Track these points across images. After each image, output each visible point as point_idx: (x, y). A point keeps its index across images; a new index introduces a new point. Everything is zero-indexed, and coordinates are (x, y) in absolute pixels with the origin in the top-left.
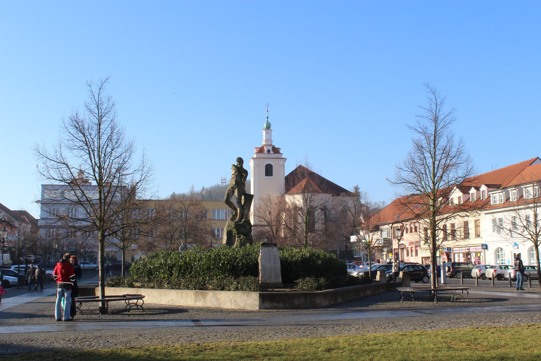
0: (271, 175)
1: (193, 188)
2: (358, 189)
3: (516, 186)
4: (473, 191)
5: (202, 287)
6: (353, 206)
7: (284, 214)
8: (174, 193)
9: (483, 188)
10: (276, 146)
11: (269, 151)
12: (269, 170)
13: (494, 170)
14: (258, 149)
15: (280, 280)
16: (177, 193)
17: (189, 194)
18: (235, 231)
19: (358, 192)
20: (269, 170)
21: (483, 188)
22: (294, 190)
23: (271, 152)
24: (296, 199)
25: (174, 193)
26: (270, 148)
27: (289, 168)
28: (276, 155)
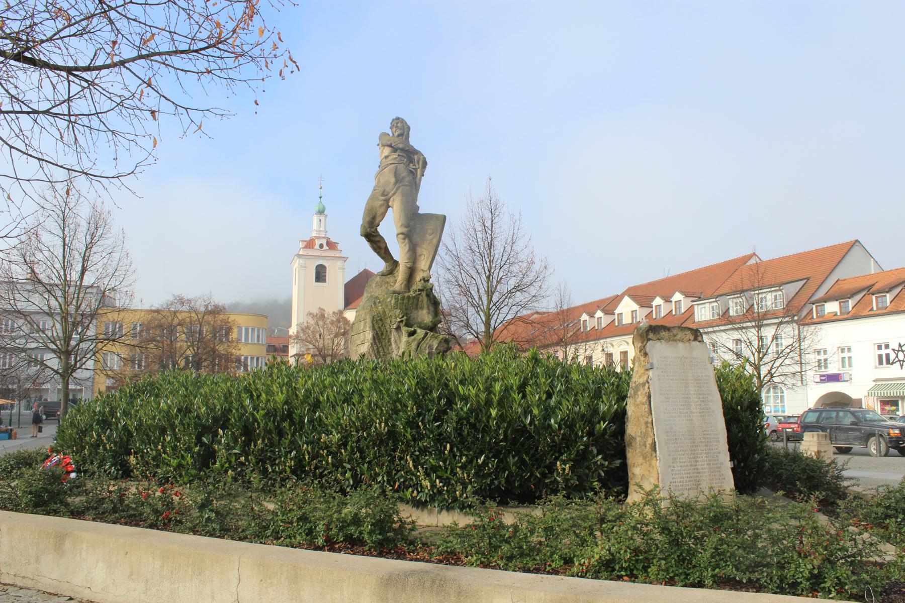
0: (324, 281)
10: (333, 240)
11: (321, 246)
12: (320, 274)
15: (729, 483)
18: (395, 316)
20: (320, 274)
23: (325, 247)
26: (324, 242)
28: (332, 253)
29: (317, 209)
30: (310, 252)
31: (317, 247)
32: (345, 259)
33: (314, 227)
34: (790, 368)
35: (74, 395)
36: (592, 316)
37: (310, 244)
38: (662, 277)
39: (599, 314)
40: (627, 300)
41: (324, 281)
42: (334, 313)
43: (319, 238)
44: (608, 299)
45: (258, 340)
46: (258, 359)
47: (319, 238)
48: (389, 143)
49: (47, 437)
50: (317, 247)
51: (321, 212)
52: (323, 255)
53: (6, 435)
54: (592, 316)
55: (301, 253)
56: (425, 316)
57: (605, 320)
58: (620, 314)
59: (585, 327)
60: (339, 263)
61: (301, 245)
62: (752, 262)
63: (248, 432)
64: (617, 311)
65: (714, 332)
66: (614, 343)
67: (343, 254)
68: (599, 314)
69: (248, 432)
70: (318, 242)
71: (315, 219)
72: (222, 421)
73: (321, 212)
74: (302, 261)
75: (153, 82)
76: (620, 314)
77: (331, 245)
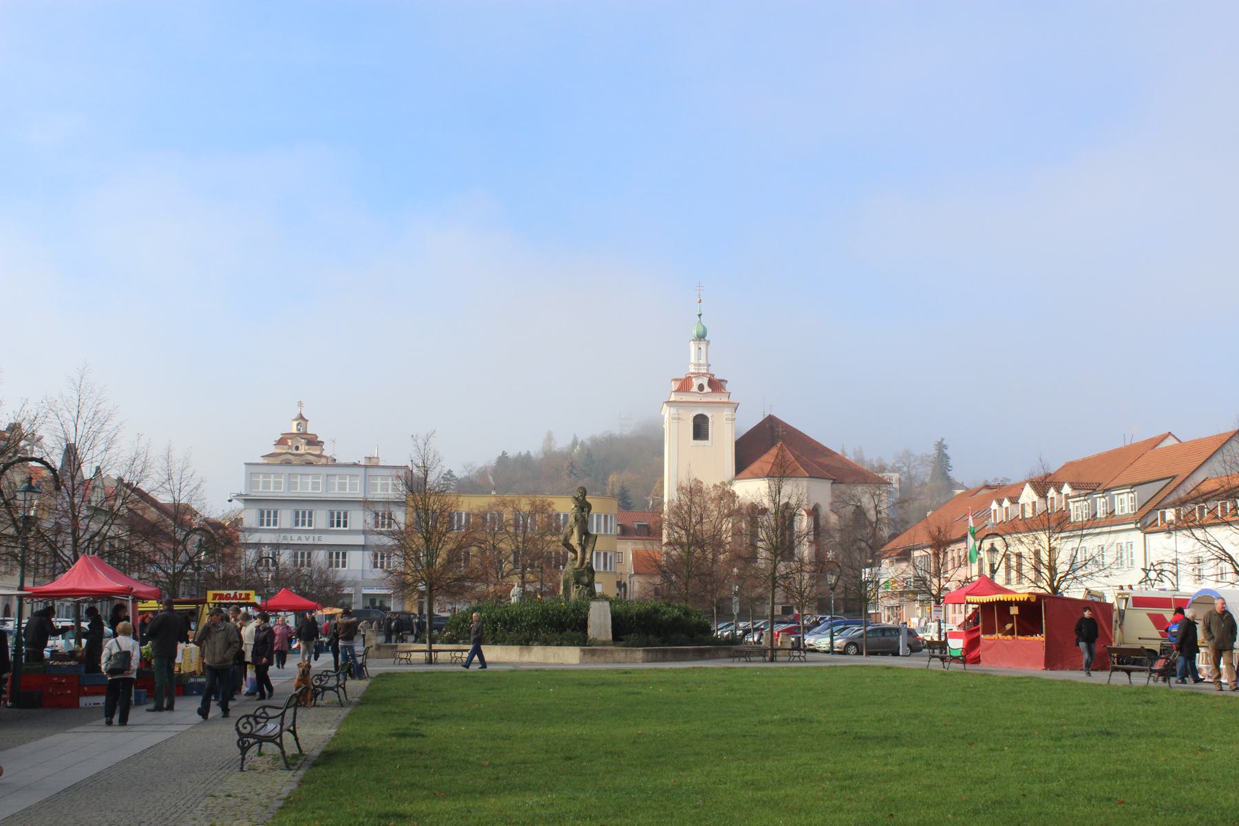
0: (706, 437)
1: (550, 438)
2: (945, 447)
3: (1133, 486)
4: (1052, 493)
5: (526, 642)
6: (872, 505)
7: (514, 600)
8: (504, 453)
9: (1066, 489)
10: (717, 377)
11: (701, 387)
12: (700, 429)
13: (1128, 443)
14: (678, 383)
15: (610, 637)
16: (512, 453)
17: (541, 456)
18: (572, 581)
19: (945, 455)
20: (700, 429)
21: (1066, 489)
22: (755, 467)
23: (707, 389)
24: (753, 490)
25: (504, 453)
26: (705, 381)
27: (749, 420)
28: (716, 398)
29: (694, 332)
30: (685, 397)
31: (695, 388)
32: (736, 407)
33: (693, 359)
35: (381, 602)
37: (684, 386)
38: (1121, 445)
41: (706, 437)
42: (715, 486)
43: (699, 375)
45: (606, 530)
46: (605, 554)
47: (699, 375)
50: (695, 388)
51: (701, 337)
52: (704, 400)
55: (673, 399)
56: (586, 580)
60: (727, 412)
61: (674, 386)
62: (1170, 442)
63: (506, 623)
64: (1021, 501)
65: (1110, 532)
67: (732, 399)
69: (506, 623)
70: (696, 382)
71: (693, 346)
72: (499, 620)
73: (701, 337)
74: (673, 410)
77: (716, 385)
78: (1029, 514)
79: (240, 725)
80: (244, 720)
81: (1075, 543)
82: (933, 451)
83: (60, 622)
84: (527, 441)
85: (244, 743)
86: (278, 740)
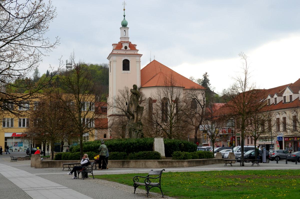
0: (128, 70)
11: (126, 48)
14: (115, 46)
23: (128, 48)
26: (127, 45)
28: (132, 52)
30: (120, 52)
31: (123, 48)
34: (263, 136)
36: (272, 96)
39: (275, 96)
40: (288, 90)
41: (128, 70)
44: (290, 84)
48: (75, 64)
49: (16, 11)
50: (123, 48)
52: (127, 53)
53: (285, 97)
54: (272, 96)
57: (279, 99)
58: (285, 97)
59: (269, 102)
64: (284, 95)
66: (280, 113)
68: (275, 96)
70: (124, 45)
75: (20, 5)
76: (285, 97)
78: (288, 100)
79: (135, 179)
80: (136, 178)
81: (153, 110)
82: (202, 78)
83: (47, 141)
84: (94, 63)
85: (148, 188)
86: (159, 186)
